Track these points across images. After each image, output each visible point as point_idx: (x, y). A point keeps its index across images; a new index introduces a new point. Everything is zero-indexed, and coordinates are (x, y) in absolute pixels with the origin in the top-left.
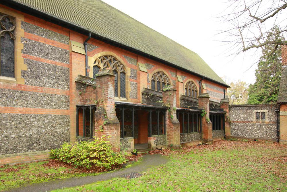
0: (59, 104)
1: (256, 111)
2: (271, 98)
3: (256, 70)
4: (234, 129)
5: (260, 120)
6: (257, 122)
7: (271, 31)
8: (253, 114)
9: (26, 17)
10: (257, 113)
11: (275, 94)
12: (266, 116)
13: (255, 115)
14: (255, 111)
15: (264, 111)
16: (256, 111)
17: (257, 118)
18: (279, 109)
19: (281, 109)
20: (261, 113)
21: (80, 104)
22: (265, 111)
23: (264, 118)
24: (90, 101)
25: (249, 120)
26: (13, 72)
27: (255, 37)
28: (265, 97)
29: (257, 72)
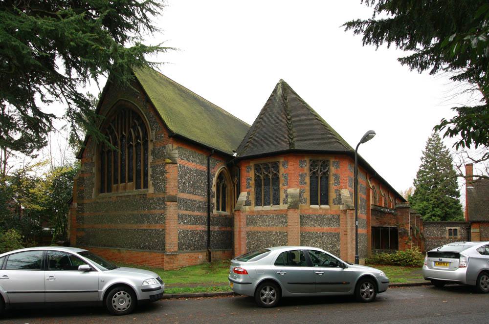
0: (199, 208)
1: (449, 228)
2: (434, 212)
3: (414, 180)
4: (428, 245)
5: (453, 237)
6: (449, 238)
7: (431, 137)
8: (446, 230)
9: (284, 157)
10: (449, 229)
11: (437, 208)
12: (458, 233)
13: (448, 232)
14: (448, 228)
15: (456, 228)
16: (449, 228)
17: (449, 235)
18: (470, 226)
19: (472, 227)
20: (454, 229)
21: (376, 225)
22: (458, 228)
23: (456, 234)
24: (389, 224)
25: (443, 236)
26: (328, 201)
27: (468, 157)
28: (428, 211)
29: (416, 183)
